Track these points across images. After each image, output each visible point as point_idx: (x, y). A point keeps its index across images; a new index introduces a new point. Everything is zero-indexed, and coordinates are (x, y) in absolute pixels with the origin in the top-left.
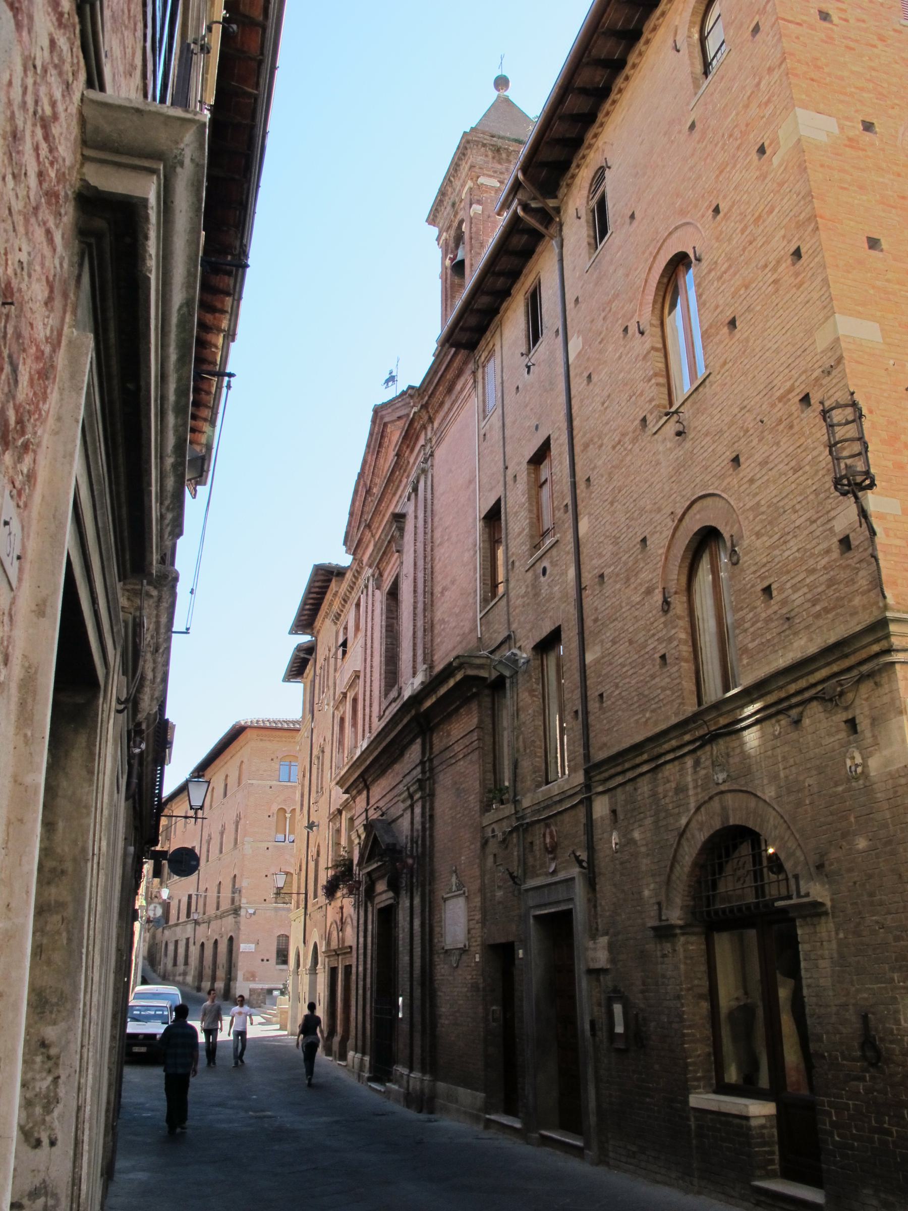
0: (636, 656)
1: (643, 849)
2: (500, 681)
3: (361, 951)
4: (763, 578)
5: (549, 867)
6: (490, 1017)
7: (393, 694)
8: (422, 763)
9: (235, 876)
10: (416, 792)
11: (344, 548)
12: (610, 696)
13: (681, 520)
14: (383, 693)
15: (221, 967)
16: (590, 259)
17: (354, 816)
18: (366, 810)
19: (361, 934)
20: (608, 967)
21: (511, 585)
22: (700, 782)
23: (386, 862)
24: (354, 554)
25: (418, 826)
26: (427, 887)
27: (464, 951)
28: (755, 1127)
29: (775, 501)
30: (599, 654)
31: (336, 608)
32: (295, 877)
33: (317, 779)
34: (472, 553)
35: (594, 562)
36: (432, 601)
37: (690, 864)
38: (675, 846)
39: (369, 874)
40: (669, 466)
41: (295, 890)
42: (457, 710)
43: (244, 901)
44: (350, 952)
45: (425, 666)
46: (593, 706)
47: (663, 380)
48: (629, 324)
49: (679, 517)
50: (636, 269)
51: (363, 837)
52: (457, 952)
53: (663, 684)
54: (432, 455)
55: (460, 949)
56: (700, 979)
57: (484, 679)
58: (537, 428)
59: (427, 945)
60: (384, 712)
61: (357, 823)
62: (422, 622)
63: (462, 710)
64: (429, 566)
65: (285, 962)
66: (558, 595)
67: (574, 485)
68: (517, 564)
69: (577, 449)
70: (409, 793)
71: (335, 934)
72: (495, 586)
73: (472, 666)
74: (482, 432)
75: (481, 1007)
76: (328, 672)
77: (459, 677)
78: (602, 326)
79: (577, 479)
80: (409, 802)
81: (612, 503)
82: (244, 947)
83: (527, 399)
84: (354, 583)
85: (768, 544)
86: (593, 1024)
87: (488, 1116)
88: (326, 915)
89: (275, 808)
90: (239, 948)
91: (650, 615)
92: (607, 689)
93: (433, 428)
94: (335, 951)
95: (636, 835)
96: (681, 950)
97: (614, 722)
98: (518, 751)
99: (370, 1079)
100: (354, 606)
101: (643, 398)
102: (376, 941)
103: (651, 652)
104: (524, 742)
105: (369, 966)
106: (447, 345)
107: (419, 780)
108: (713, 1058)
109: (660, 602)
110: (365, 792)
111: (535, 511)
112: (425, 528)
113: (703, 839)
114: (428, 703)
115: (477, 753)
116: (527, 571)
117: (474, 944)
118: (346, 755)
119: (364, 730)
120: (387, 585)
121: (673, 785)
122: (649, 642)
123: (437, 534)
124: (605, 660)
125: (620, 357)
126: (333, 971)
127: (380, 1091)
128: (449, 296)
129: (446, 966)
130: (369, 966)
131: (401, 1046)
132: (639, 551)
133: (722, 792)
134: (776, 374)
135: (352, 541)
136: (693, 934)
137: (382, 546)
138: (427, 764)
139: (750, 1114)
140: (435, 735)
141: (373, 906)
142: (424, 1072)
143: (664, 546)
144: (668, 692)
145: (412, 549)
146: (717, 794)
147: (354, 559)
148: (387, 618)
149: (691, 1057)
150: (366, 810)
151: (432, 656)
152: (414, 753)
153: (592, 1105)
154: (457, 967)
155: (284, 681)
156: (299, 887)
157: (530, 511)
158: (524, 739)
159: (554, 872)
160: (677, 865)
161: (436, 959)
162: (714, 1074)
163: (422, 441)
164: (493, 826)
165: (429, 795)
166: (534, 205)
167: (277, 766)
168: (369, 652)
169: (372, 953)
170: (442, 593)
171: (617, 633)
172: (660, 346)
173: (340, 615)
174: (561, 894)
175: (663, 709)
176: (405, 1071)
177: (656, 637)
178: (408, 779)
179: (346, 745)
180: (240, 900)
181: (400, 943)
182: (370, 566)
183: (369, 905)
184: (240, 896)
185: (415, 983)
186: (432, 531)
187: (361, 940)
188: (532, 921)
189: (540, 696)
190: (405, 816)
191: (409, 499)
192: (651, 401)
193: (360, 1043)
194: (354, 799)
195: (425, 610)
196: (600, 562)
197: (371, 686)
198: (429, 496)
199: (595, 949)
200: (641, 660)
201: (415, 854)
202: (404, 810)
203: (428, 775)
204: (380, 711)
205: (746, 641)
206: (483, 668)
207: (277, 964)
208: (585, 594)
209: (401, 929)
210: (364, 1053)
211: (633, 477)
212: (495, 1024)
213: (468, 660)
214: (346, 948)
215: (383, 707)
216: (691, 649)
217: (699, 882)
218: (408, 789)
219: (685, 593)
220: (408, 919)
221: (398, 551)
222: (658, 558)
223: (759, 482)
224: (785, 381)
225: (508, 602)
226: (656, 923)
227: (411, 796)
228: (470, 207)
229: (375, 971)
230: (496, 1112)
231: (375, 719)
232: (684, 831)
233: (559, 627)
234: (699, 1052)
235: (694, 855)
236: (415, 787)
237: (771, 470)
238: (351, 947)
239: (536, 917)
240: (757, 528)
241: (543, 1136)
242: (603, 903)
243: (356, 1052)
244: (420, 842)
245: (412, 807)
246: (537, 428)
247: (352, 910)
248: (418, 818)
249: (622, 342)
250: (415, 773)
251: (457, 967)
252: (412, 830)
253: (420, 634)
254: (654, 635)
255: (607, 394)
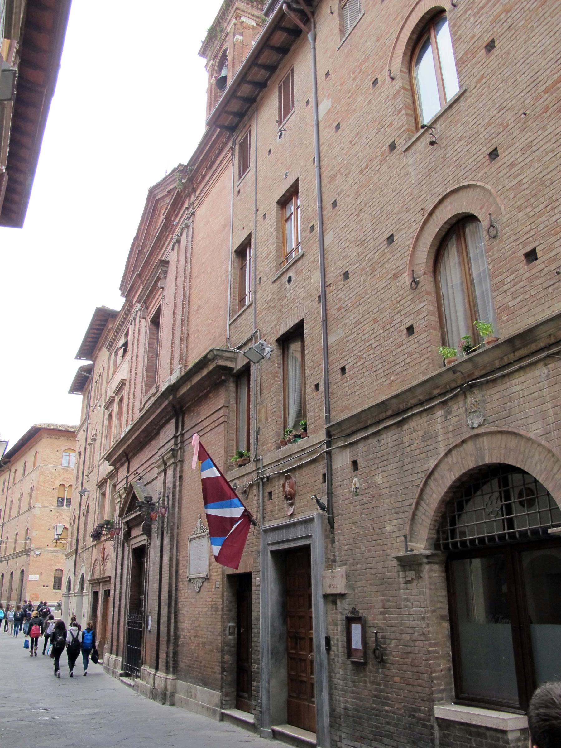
0: (381, 331)
1: (386, 491)
2: (246, 371)
3: (118, 579)
4: (525, 245)
5: (287, 511)
6: (227, 632)
7: (153, 390)
8: (175, 437)
9: (28, 529)
10: (169, 459)
11: (120, 292)
12: (351, 369)
13: (431, 214)
14: (144, 391)
15: (5, 591)
16: (341, 40)
17: (116, 482)
18: (127, 477)
19: (119, 567)
20: (346, 592)
21: (258, 295)
22: (451, 428)
23: (143, 511)
24: (128, 296)
25: (170, 485)
26: (176, 531)
27: (206, 579)
28: (512, 741)
29: (540, 176)
30: (342, 335)
31: (110, 338)
32: (70, 530)
33: (90, 459)
34: (224, 277)
35: (338, 264)
36: (188, 318)
37: (438, 501)
38: (421, 486)
39: (127, 523)
40: (418, 174)
41: (69, 537)
42: (209, 392)
43: (33, 546)
44: (110, 581)
45: (180, 366)
46: (336, 376)
47: (411, 112)
48: (379, 76)
49: (429, 211)
50: (387, 34)
51: (123, 496)
52: (200, 581)
53: (410, 349)
54: (193, 214)
55: (202, 578)
56: (441, 602)
57: (231, 369)
58: (286, 175)
59: (174, 574)
60: (144, 405)
61: (118, 487)
62: (180, 333)
63: (211, 395)
64: (188, 293)
65: (59, 588)
66: (302, 296)
67: (321, 208)
68: (264, 279)
69: (325, 181)
70: (163, 460)
71: (98, 567)
72: (242, 301)
73: (223, 358)
74: (237, 189)
75: (219, 623)
76: (102, 384)
77: (211, 367)
78: (352, 85)
79: (324, 203)
80: (163, 468)
81: (358, 215)
82: (32, 577)
83: (279, 156)
84: (125, 319)
85: (531, 214)
86: (328, 640)
87: (223, 711)
88: (92, 554)
89: (58, 483)
90: (28, 578)
91: (397, 295)
92: (348, 362)
93: (195, 195)
94: (97, 579)
95: (379, 479)
96: (427, 577)
97: (357, 388)
98: (260, 421)
99: (121, 675)
100: (123, 335)
101: (391, 128)
102: (130, 572)
103: (398, 325)
104: (266, 414)
105: (124, 590)
106: (214, 127)
107: (172, 450)
108: (452, 672)
109: (408, 283)
110: (126, 464)
111: (281, 239)
112: (185, 266)
113: (453, 478)
114: (183, 390)
115: (223, 425)
116: (274, 282)
117: (215, 574)
118: (112, 440)
119: (127, 420)
120: (151, 316)
121: (421, 433)
122: (395, 317)
123: (195, 270)
124: (348, 338)
125: (369, 103)
126: (96, 594)
127: (130, 685)
128: (213, 103)
129: (189, 591)
130: (124, 590)
131: (148, 651)
132: (385, 246)
133: (477, 436)
134: (542, 71)
135: (126, 287)
136: (435, 563)
137: (149, 286)
138: (179, 438)
139: (508, 728)
140: (186, 416)
141: (129, 547)
142: (167, 671)
143: (413, 238)
144: (416, 356)
145: (174, 284)
146: (471, 438)
147: (126, 301)
148: (150, 338)
149: (435, 672)
150: (127, 477)
151: (187, 358)
152: (169, 431)
153: (326, 709)
154: (199, 592)
155: (69, 392)
156: (72, 535)
157: (278, 238)
158: (266, 411)
159: (292, 515)
160: (423, 503)
161: (180, 585)
162: (453, 686)
163: (186, 205)
164: (235, 481)
165: (179, 461)
166: (295, 6)
167: (61, 456)
168: (134, 364)
169: (127, 581)
170: (197, 311)
171: (361, 315)
172: (408, 87)
173: (113, 343)
174: (300, 532)
175: (410, 371)
176: (153, 671)
177: (403, 313)
178: (163, 450)
179: (113, 433)
180: (30, 546)
181: (151, 573)
182: (139, 302)
183: (126, 544)
184: (31, 543)
185: (162, 604)
186: (191, 268)
187: (119, 571)
188: (269, 555)
189: (281, 378)
190: (159, 478)
191: (173, 249)
192: (400, 128)
193: (114, 648)
194: (117, 470)
195: (182, 325)
196: (345, 263)
197: (135, 388)
198: (190, 243)
199: (333, 577)
200: (385, 334)
201: (166, 505)
202: (159, 474)
203: (179, 445)
204: (141, 405)
205: (507, 300)
206: (231, 361)
207: (54, 588)
208: (328, 290)
209: (151, 562)
210: (117, 655)
211: (380, 190)
212: (231, 637)
213: (220, 353)
214: (106, 577)
215: (144, 401)
216: (437, 320)
217: (444, 517)
218: (163, 457)
219: (432, 275)
220: (159, 555)
221: (162, 288)
222: (407, 248)
223: (519, 166)
224: (554, 74)
225: (255, 309)
226: (402, 553)
227: (165, 463)
228: (234, 37)
229: (129, 594)
230: (230, 708)
231: (137, 411)
232: (432, 473)
233: (303, 320)
234: (442, 667)
235: (443, 493)
236: (170, 455)
237: (534, 152)
238: (110, 577)
239: (272, 552)
240: (519, 203)
241: (273, 731)
242: (341, 538)
243: (111, 653)
244: (171, 496)
245: (165, 471)
246: (286, 175)
247: (112, 549)
248: (170, 479)
249: (371, 91)
250: (169, 445)
251: (199, 592)
252: (164, 488)
253: (177, 342)
254: (400, 311)
255: (355, 133)
